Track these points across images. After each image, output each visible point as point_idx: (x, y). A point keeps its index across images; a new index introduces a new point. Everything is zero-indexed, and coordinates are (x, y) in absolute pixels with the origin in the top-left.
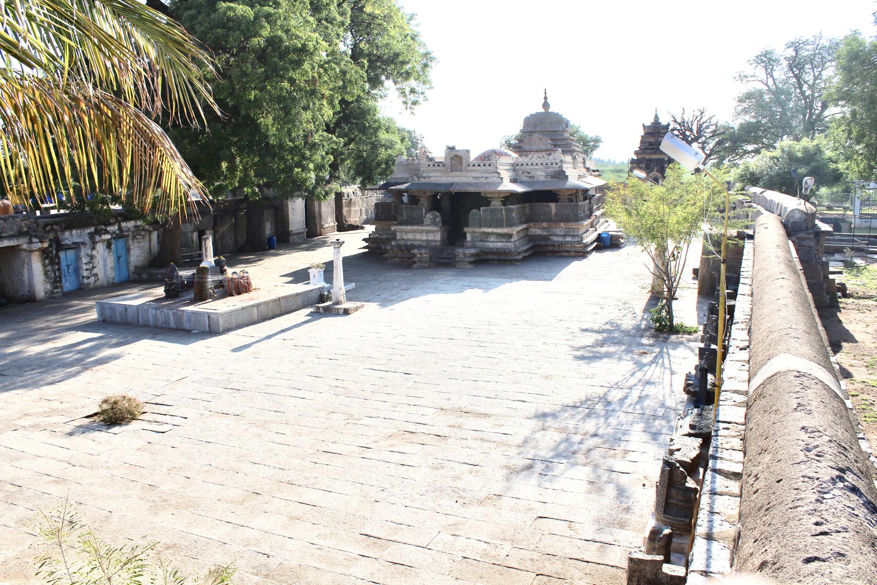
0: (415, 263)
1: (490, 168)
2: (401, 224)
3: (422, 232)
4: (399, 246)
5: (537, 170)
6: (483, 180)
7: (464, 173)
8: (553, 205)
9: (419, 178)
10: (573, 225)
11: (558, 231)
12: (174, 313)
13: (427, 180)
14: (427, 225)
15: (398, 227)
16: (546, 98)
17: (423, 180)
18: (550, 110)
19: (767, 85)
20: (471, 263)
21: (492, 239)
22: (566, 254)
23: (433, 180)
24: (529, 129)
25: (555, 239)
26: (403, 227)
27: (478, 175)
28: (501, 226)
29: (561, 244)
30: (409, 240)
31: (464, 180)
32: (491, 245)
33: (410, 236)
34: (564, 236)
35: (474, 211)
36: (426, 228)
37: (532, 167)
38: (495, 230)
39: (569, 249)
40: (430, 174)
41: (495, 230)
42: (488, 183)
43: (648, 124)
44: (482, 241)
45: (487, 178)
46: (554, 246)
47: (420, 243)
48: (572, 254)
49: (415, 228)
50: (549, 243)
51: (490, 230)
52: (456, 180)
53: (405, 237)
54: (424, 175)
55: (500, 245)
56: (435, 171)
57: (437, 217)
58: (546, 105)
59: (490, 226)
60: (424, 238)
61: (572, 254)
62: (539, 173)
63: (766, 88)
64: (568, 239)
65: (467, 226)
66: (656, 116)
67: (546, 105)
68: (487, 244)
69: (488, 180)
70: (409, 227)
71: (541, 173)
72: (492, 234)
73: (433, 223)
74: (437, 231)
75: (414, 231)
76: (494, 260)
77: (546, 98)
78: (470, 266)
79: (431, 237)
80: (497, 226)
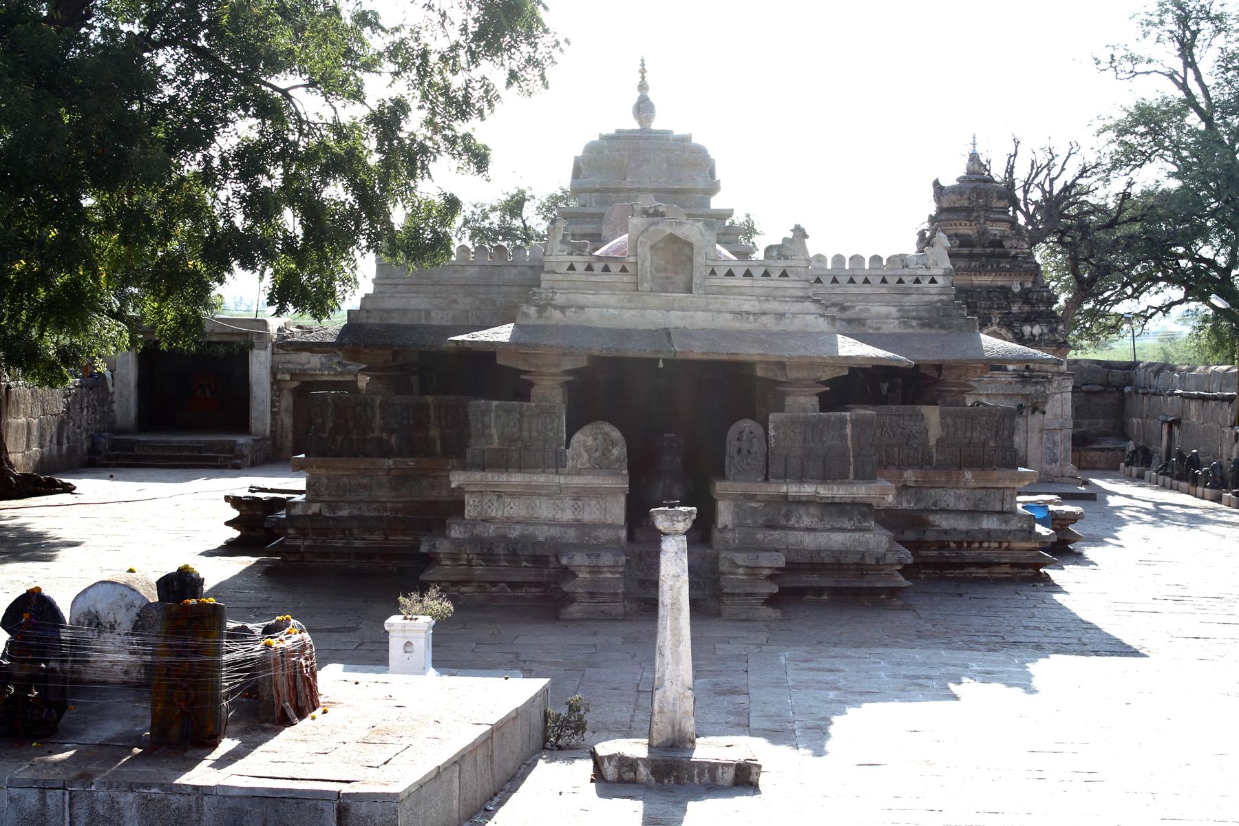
0: (569, 599)
1: (785, 283)
2: (483, 467)
3: (555, 494)
4: (476, 540)
5: (867, 298)
6: (769, 322)
7: (696, 298)
8: (932, 414)
9: (542, 309)
10: (1000, 478)
11: (949, 498)
12: (146, 803)
13: (572, 318)
14: (579, 473)
15: (478, 476)
16: (643, 87)
17: (556, 316)
18: (656, 125)
19: (1183, 86)
20: (772, 601)
21: (806, 521)
22: (982, 572)
23: (593, 317)
24: (598, 181)
25: (945, 522)
26: (493, 477)
27: (747, 307)
28: (840, 477)
29: (968, 540)
30: (509, 521)
31: (700, 319)
32: (809, 541)
33: (515, 509)
34: (974, 513)
35: (746, 424)
36: (577, 481)
37: (852, 289)
38: (824, 491)
39: (993, 557)
40: (580, 299)
41: (824, 491)
42: (785, 333)
43: (949, 180)
44: (770, 526)
45: (781, 316)
46: (943, 545)
47: (553, 532)
48: (998, 572)
49: (539, 479)
50: (931, 536)
51: (808, 489)
52: (676, 319)
53: (496, 511)
54: (560, 299)
55: (838, 540)
56: (597, 287)
57: (613, 444)
58: (643, 108)
59: (801, 478)
60: (567, 516)
61: (998, 572)
62: (878, 309)
63: (1181, 94)
64: (989, 523)
65: (722, 475)
66: (974, 158)
67: (643, 108)
68: (793, 537)
69: (789, 325)
70: (517, 478)
71: (884, 310)
72: (800, 502)
73: (601, 465)
74: (613, 492)
75: (531, 492)
76: (819, 591)
77: (643, 87)
78: (769, 612)
79: (591, 514)
80: (825, 477)
